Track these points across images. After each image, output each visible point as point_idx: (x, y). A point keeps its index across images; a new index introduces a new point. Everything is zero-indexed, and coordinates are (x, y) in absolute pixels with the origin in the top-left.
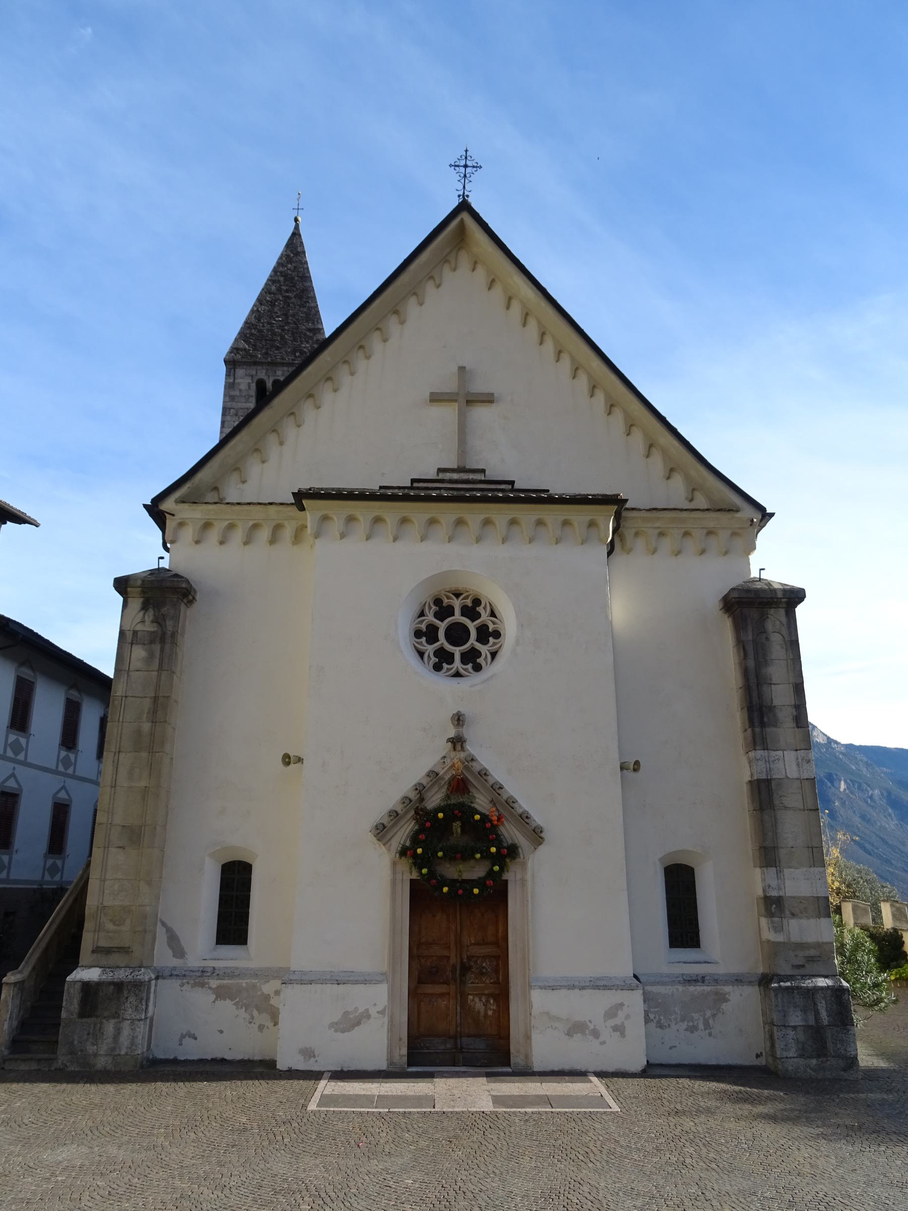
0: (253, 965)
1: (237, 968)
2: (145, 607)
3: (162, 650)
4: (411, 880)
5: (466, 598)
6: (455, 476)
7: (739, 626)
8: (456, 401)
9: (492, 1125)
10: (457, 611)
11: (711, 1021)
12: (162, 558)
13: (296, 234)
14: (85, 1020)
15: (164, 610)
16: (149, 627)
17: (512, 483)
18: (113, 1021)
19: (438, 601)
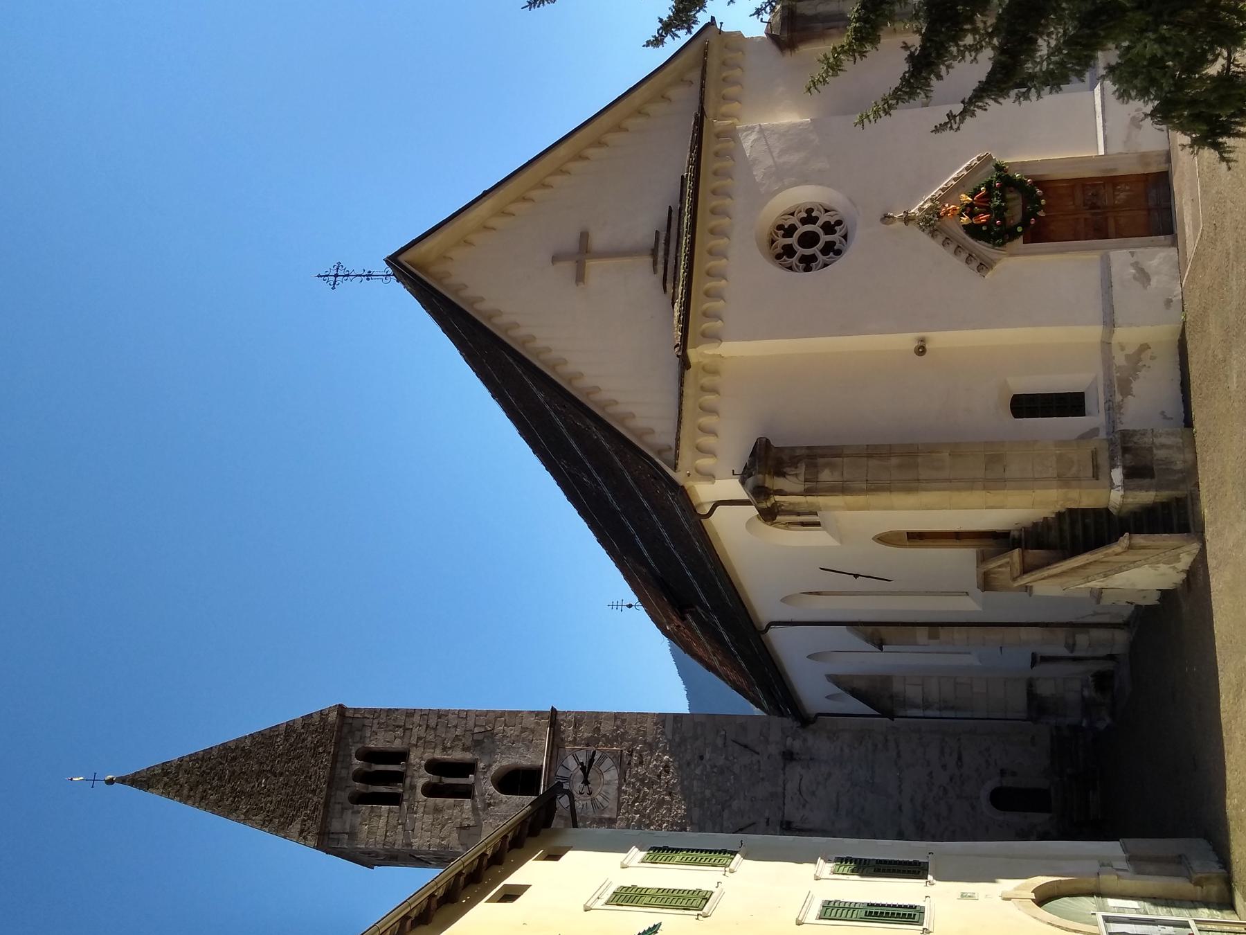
2: (783, 475)
3: (823, 456)
16: (802, 469)
18: (1155, 451)
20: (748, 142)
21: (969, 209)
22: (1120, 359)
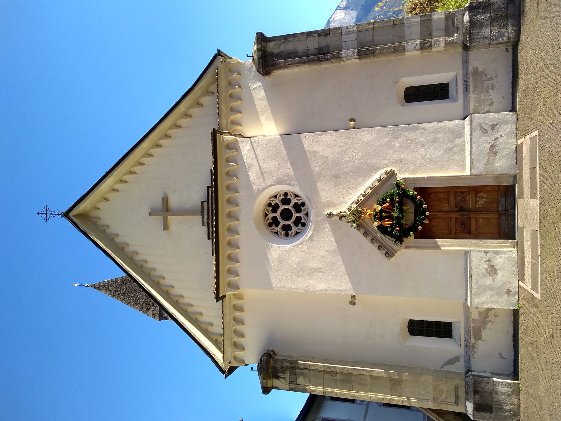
0: (462, 321)
1: (464, 329)
2: (277, 377)
3: (300, 368)
4: (416, 238)
5: (268, 210)
6: (206, 217)
7: (276, 67)
8: (167, 217)
9: (547, 202)
10: (275, 215)
11: (489, 76)
12: (252, 368)
13: (95, 287)
14: (494, 410)
15: (278, 367)
16: (288, 375)
17: (208, 188)
19: (270, 225)
20: (245, 148)
21: (379, 216)
22: (475, 315)
